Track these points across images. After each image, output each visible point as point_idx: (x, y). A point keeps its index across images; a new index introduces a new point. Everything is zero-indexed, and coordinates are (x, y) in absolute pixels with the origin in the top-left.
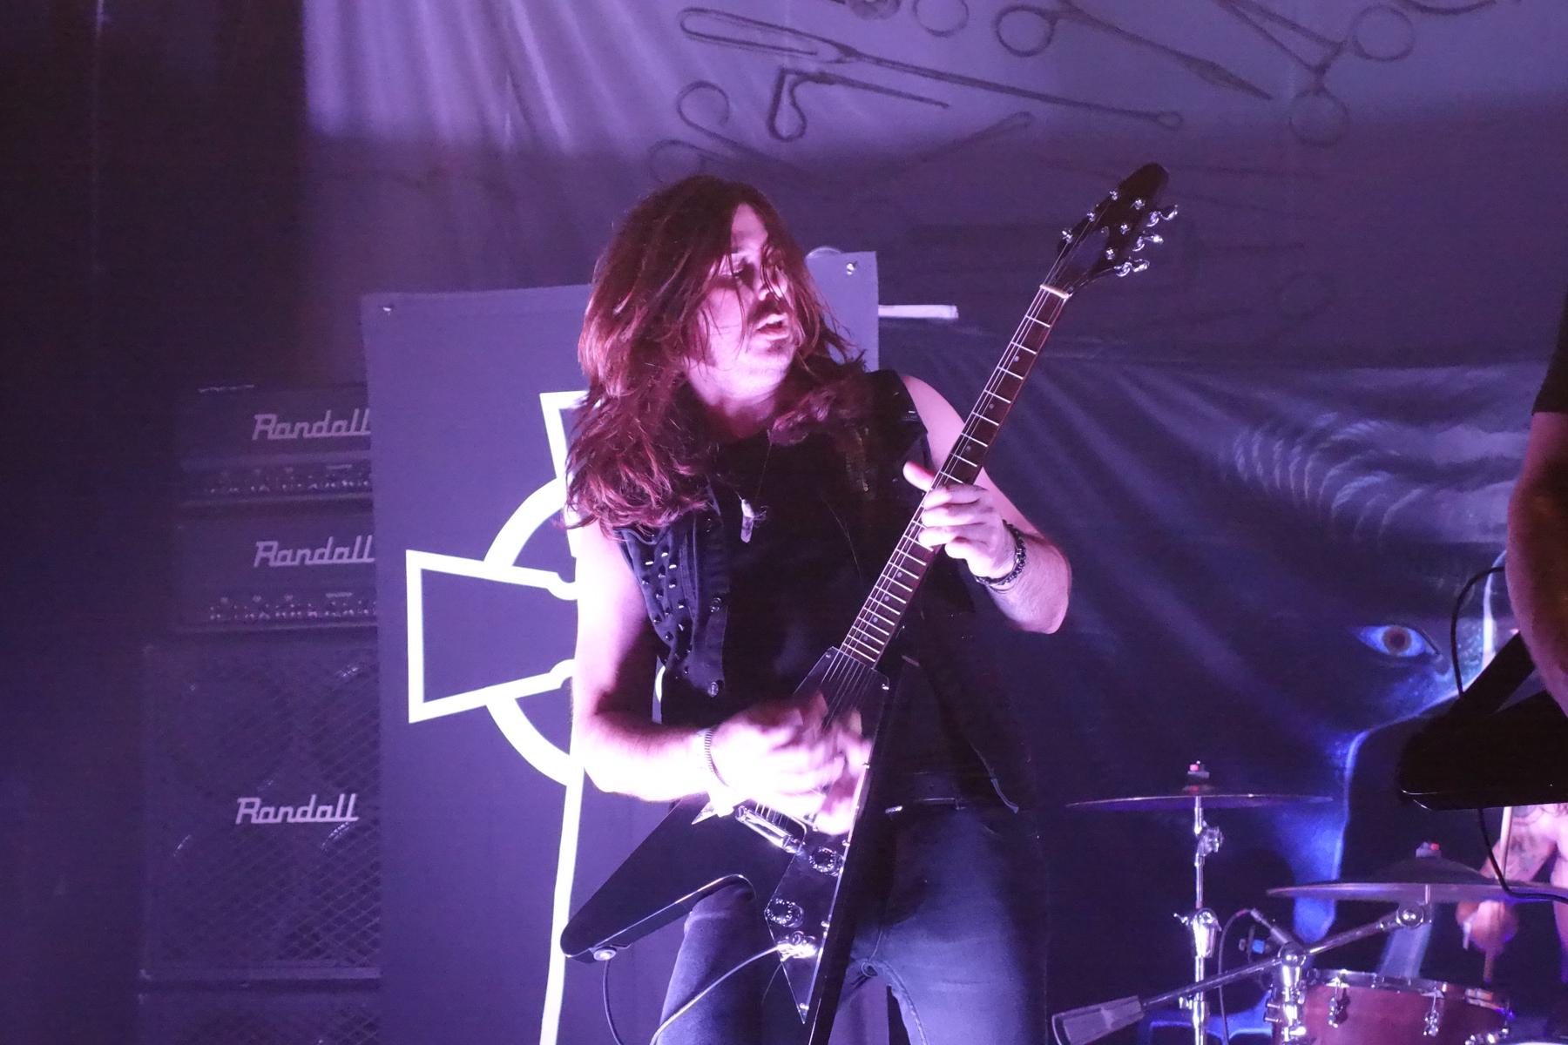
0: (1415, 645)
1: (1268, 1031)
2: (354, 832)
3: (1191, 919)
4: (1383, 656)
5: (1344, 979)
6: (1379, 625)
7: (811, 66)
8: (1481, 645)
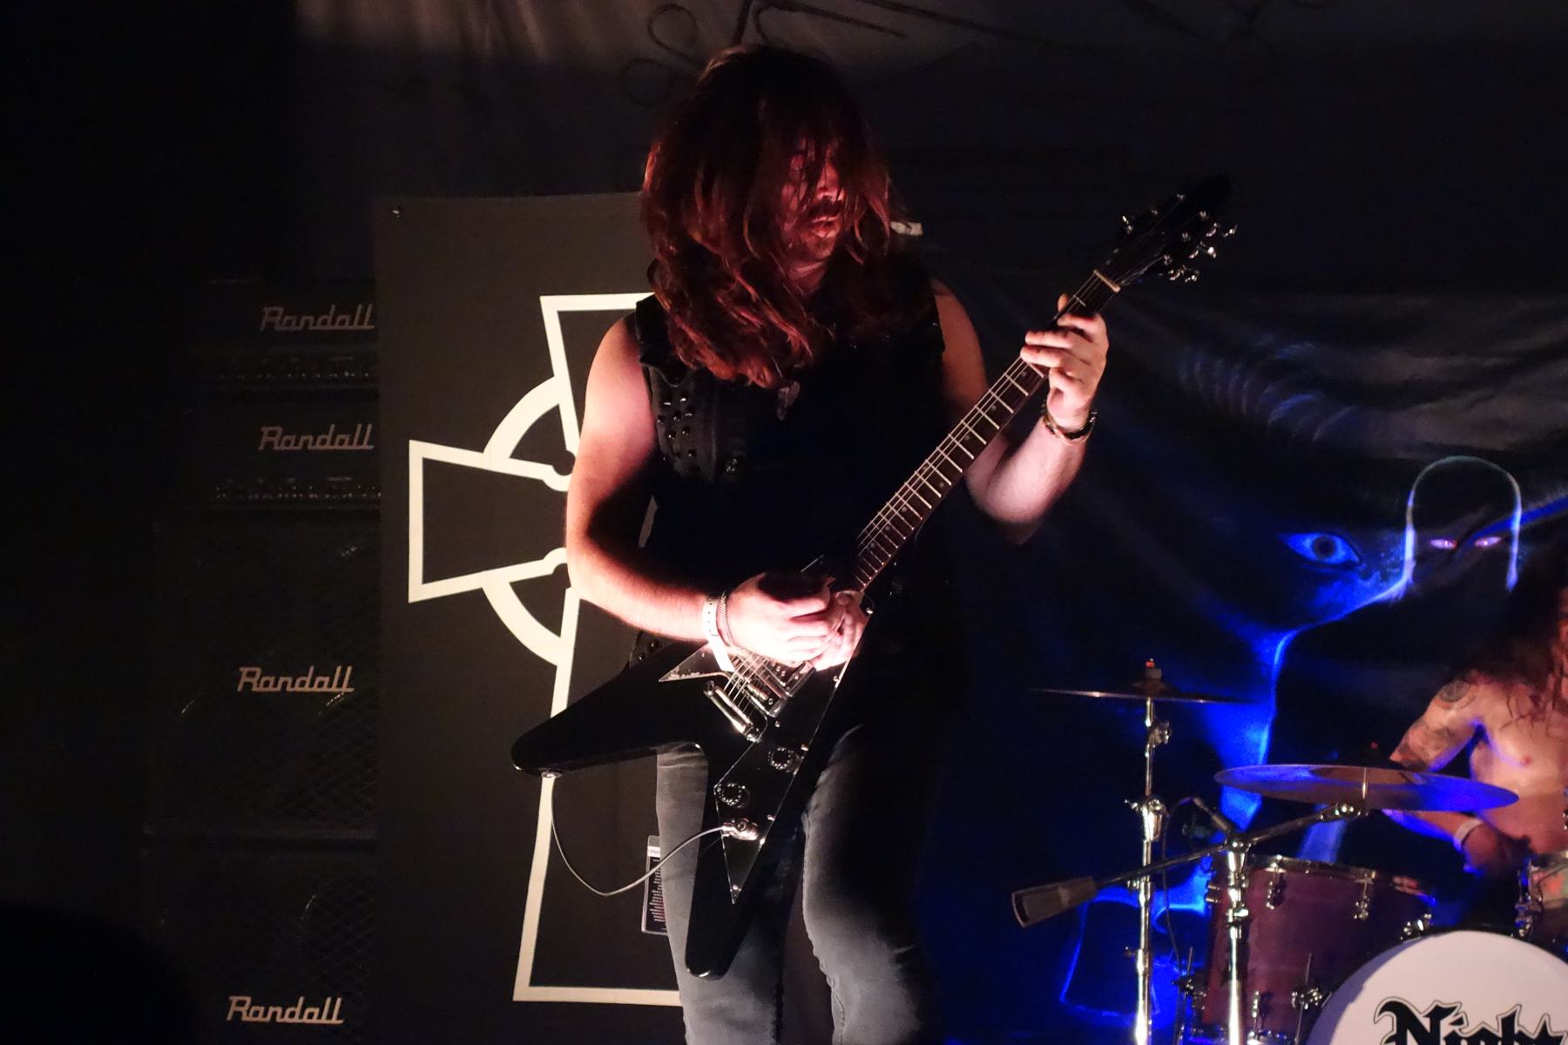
0: (1341, 553)
2: (348, 703)
3: (1140, 805)
4: (1313, 563)
5: (1281, 864)
6: (1308, 532)
8: (1403, 552)
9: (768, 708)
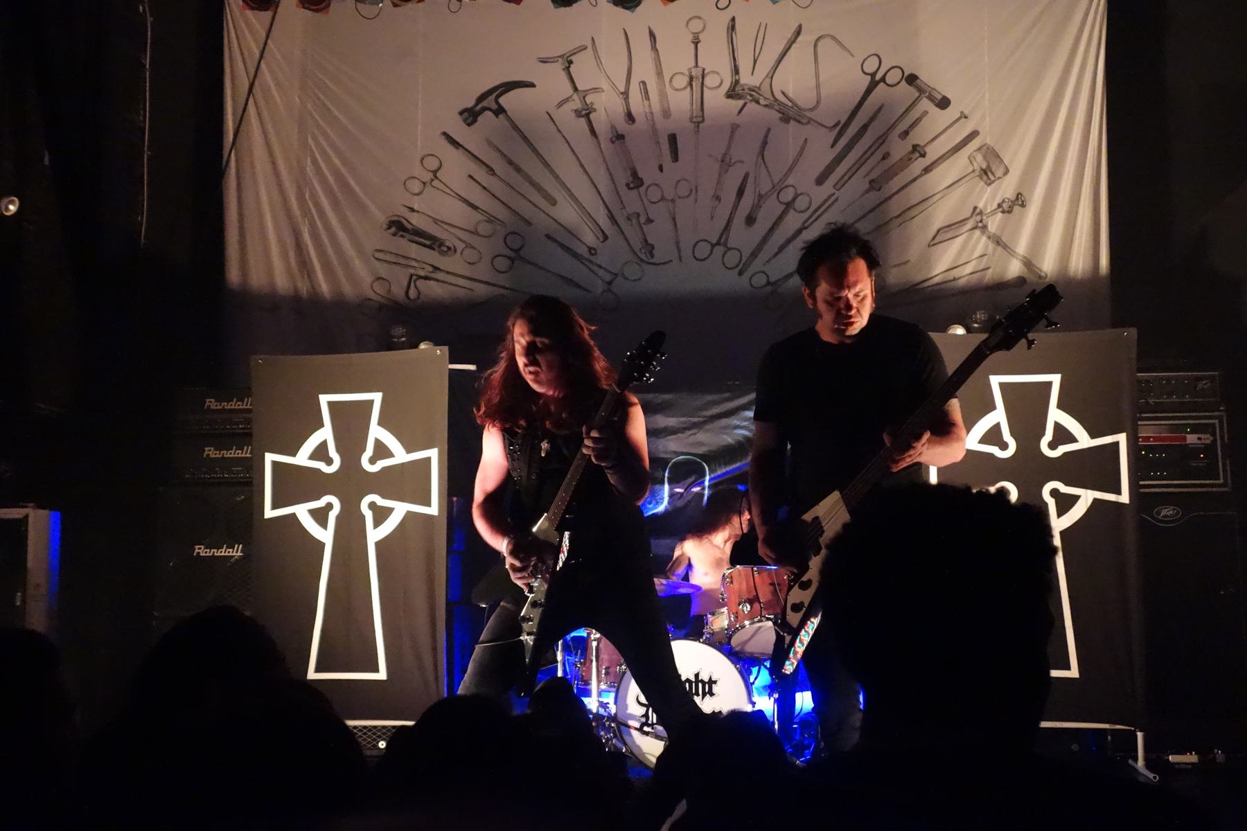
1: (585, 635)
7: (422, 273)
9: (856, 295)
